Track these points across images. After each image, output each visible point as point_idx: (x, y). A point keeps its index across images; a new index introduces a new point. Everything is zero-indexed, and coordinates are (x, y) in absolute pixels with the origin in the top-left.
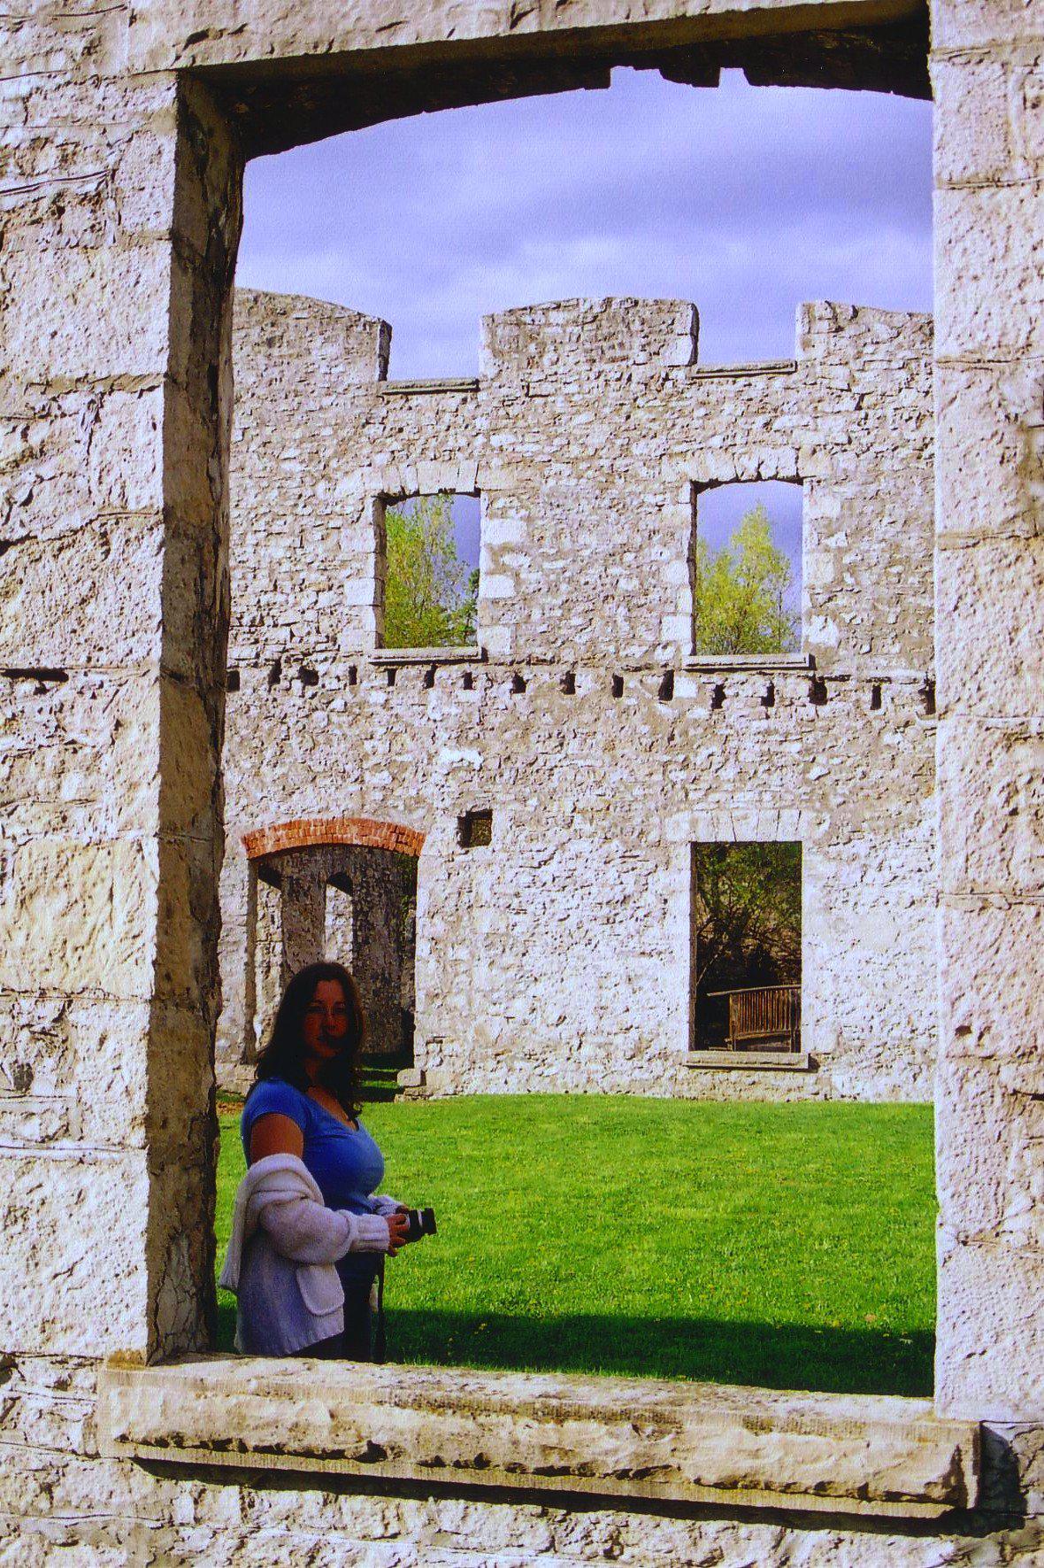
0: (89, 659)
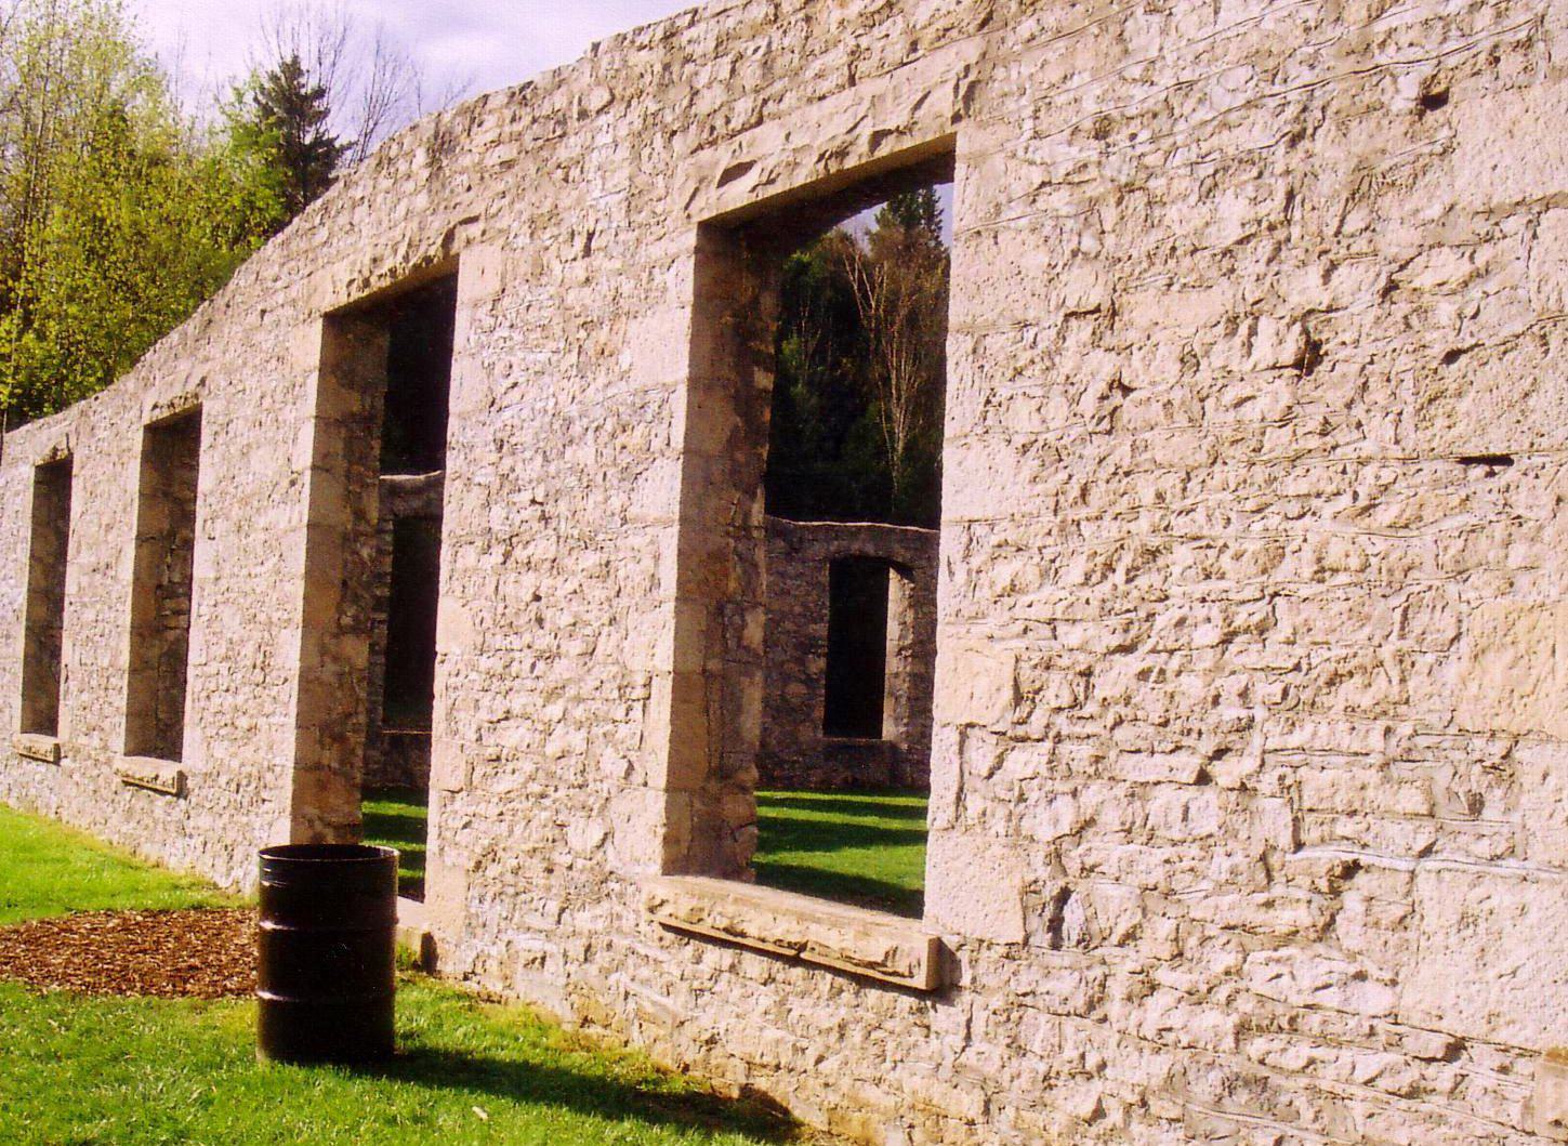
0: (1532, 445)
